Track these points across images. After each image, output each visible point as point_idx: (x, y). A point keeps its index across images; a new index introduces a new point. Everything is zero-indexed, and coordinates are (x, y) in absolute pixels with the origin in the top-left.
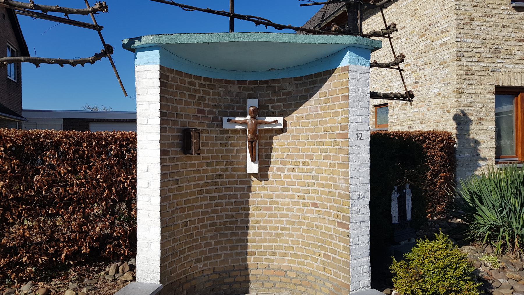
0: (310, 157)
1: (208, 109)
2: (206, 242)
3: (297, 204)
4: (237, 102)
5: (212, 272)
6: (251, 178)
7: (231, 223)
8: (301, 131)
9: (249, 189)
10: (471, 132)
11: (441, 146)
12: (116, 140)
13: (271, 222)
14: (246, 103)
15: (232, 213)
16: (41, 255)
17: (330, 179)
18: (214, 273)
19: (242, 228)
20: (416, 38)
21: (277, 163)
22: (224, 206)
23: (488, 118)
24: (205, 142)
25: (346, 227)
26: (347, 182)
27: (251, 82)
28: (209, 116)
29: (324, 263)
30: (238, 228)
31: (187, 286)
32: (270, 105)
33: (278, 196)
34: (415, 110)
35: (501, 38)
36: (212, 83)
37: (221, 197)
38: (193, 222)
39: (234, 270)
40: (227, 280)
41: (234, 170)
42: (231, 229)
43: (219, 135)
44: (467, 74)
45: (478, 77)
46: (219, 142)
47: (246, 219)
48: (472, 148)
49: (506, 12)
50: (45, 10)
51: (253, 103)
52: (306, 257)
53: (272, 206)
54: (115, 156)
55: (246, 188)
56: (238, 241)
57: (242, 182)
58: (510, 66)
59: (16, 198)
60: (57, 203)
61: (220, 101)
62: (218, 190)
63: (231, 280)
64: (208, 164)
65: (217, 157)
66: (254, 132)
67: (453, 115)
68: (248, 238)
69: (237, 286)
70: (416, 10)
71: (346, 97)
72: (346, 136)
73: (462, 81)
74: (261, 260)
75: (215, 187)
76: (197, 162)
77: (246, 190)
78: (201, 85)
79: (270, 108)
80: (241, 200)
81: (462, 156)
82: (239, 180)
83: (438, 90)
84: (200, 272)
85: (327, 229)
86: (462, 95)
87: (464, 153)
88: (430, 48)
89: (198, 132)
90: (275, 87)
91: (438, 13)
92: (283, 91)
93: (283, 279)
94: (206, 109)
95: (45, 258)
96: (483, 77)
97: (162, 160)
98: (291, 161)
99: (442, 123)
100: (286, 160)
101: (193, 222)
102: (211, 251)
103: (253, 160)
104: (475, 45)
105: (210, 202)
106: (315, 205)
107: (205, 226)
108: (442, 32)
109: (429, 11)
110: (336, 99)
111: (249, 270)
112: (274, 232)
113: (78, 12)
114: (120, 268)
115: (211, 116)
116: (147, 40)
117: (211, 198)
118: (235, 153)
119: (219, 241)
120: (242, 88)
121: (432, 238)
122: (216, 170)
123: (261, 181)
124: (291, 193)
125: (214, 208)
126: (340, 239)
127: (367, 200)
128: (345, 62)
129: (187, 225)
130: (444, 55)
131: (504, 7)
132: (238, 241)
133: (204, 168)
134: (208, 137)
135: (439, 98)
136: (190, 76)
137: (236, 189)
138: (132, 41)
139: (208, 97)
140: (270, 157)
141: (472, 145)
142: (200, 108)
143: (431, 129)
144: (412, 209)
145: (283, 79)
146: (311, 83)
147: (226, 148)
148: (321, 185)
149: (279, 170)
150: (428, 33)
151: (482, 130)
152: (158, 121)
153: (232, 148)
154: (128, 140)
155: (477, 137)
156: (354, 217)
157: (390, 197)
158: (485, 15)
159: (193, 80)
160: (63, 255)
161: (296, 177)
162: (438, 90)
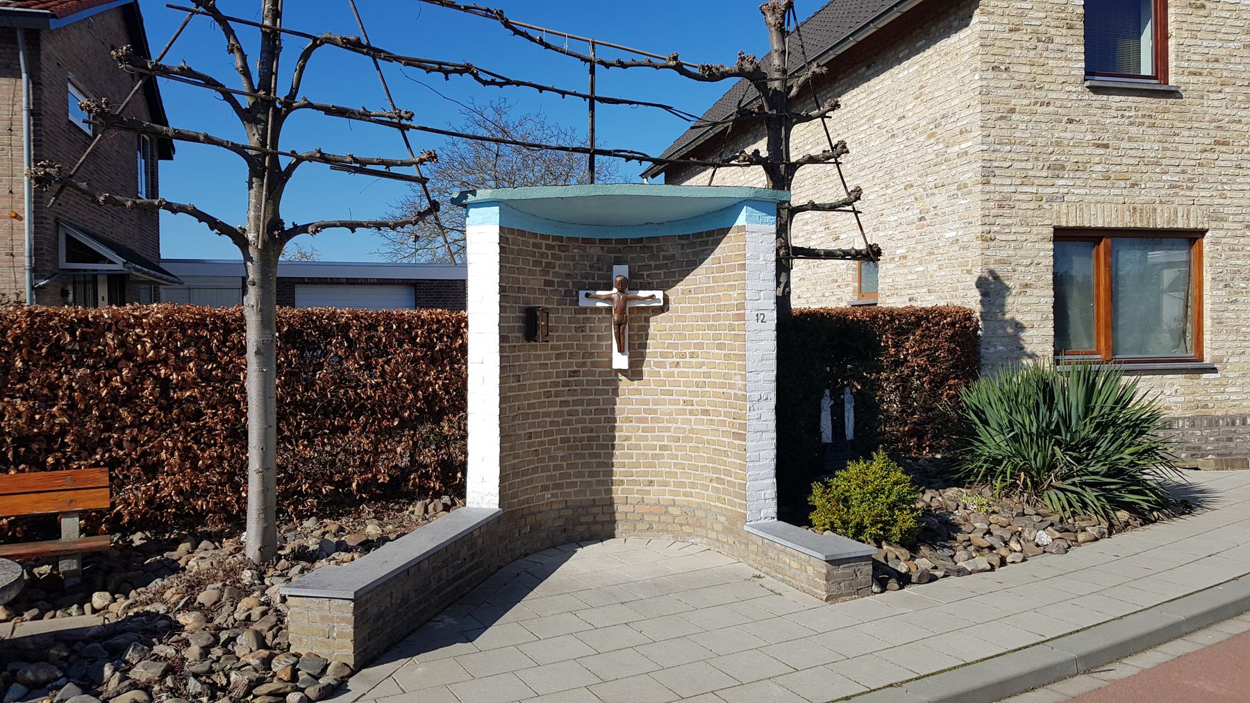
0: (700, 346)
3: (683, 412)
5: (563, 505)
7: (590, 439)
8: (688, 310)
9: (616, 392)
10: (1008, 308)
11: (950, 332)
12: (423, 321)
13: (646, 439)
14: (611, 270)
16: (324, 484)
17: (724, 376)
18: (567, 507)
19: (605, 447)
20: (922, 139)
23: (1041, 284)
25: (742, 437)
26: (744, 378)
27: (618, 241)
29: (716, 490)
30: (600, 447)
31: (530, 519)
33: (656, 402)
34: (921, 269)
35: (1066, 142)
37: (575, 403)
38: (538, 435)
40: (582, 519)
41: (594, 365)
44: (1000, 207)
45: (1021, 212)
48: (1009, 336)
49: (1074, 96)
50: (364, 163)
51: (620, 271)
52: (693, 485)
54: (422, 345)
56: (599, 465)
57: (605, 383)
58: (1083, 191)
59: (294, 402)
60: (345, 411)
62: (573, 393)
63: (590, 519)
64: (558, 356)
65: (571, 346)
67: (976, 279)
69: (598, 527)
70: (922, 87)
71: (743, 267)
72: (742, 317)
73: (991, 220)
74: (632, 492)
78: (549, 247)
81: (992, 350)
83: (954, 234)
85: (722, 444)
86: (992, 244)
87: (995, 346)
88: (942, 159)
89: (547, 312)
91: (955, 98)
93: (663, 518)
94: (556, 280)
95: (329, 487)
96: (1030, 212)
97: (502, 349)
99: (961, 293)
101: (538, 435)
102: (562, 476)
103: (621, 350)
104: (1016, 157)
106: (706, 412)
107: (553, 442)
108: (961, 133)
109: (942, 92)
110: (731, 268)
112: (650, 452)
113: (403, 164)
114: (431, 507)
116: (483, 194)
117: (563, 403)
121: (868, 457)
126: (737, 456)
127: (772, 403)
128: (741, 220)
129: (530, 438)
130: (964, 173)
131: (1071, 88)
132: (599, 465)
134: (559, 317)
135: (956, 248)
136: (535, 235)
137: (597, 392)
138: (463, 195)
139: (558, 263)
140: (645, 346)
141: (1010, 330)
143: (942, 304)
144: (856, 424)
146: (702, 243)
148: (714, 385)
149: (657, 364)
150: (939, 130)
151: (1027, 305)
152: (497, 298)
154: (439, 322)
155: (1019, 318)
156: (753, 425)
157: (819, 404)
158: (1036, 103)
159: (538, 241)
160: (354, 485)
161: (681, 374)
162: (954, 234)
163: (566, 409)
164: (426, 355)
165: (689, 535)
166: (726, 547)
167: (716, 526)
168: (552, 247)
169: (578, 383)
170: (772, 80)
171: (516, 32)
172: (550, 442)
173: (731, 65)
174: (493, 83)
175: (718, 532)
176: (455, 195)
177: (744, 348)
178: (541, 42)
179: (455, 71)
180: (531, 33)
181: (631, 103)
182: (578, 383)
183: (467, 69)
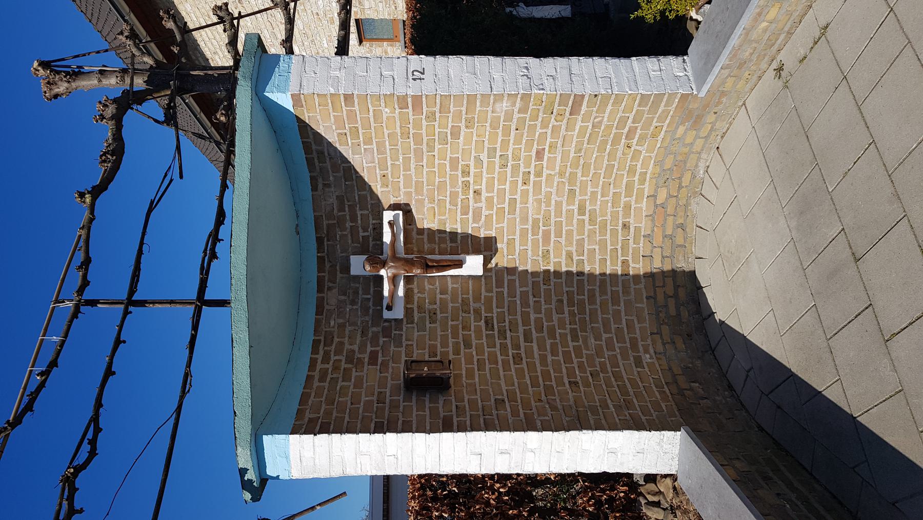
0: (454, 163)
1: (369, 345)
3: (537, 185)
4: (356, 292)
5: (657, 337)
7: (571, 303)
8: (408, 178)
9: (511, 271)
12: (423, 507)
13: (569, 233)
14: (357, 278)
15: (553, 303)
18: (659, 333)
19: (580, 284)
21: (464, 222)
22: (542, 316)
24: (427, 350)
26: (499, 98)
27: (320, 269)
28: (381, 342)
29: (642, 138)
30: (580, 290)
31: (682, 380)
33: (525, 220)
36: (322, 338)
37: (526, 322)
38: (571, 372)
41: (477, 299)
42: (581, 303)
46: (428, 325)
51: (358, 265)
52: (632, 171)
53: (541, 231)
55: (510, 277)
56: (603, 292)
57: (500, 284)
62: (513, 326)
63: (672, 303)
64: (468, 345)
66: (409, 263)
68: (598, 273)
71: (348, 98)
72: (417, 99)
75: (508, 332)
76: (463, 365)
77: (513, 278)
78: (326, 359)
79: (366, 234)
80: (530, 286)
82: (495, 290)
84: (658, 359)
90: (328, 226)
92: (335, 211)
93: (670, 210)
97: (462, 428)
98: (461, 197)
100: (459, 206)
101: (571, 372)
102: (621, 339)
103: (459, 264)
106: (540, 154)
107: (578, 350)
110: (351, 115)
111: (655, 271)
112: (587, 227)
114: (651, 498)
115: (382, 340)
116: (244, 459)
117: (528, 337)
118: (448, 297)
120: (331, 285)
123: (496, 250)
124: (518, 197)
125: (545, 334)
126: (601, 110)
128: (284, 100)
129: (576, 383)
132: (603, 292)
133: (474, 353)
134: (419, 346)
136: (309, 378)
137: (512, 294)
138: (247, 485)
140: (453, 235)
145: (314, 211)
147: (438, 312)
152: (391, 437)
153: (438, 302)
156: (562, 86)
157: (525, 19)
159: (316, 374)
161: (490, 188)
163: (535, 335)
164: (464, 504)
165: (694, 177)
166: (718, 125)
167: (688, 140)
170: (132, 84)
171: (29, 407)
172: (579, 355)
173: (108, 128)
174: (93, 442)
175: (697, 137)
176: (247, 496)
177: (459, 98)
178: (46, 373)
179: (71, 499)
180: (32, 388)
181: (140, 252)
183: (69, 483)
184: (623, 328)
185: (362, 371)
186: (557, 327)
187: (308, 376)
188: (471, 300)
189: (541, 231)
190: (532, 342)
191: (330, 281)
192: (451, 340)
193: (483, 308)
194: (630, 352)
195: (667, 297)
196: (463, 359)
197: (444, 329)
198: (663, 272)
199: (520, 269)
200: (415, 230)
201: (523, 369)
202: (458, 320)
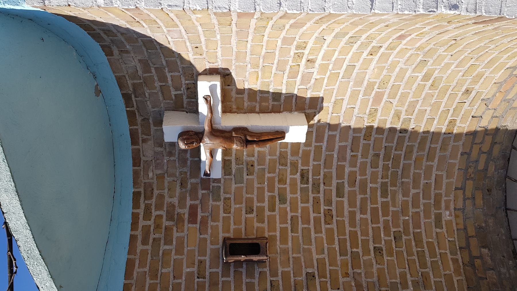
1: (188, 198)
2: (410, 205)
5: (460, 192)
6: (313, 125)
7: (387, 157)
9: (332, 127)
15: (370, 157)
18: (463, 188)
22: (357, 169)
24: (244, 205)
28: (200, 196)
31: (474, 242)
32: (173, 93)
36: (142, 190)
37: (340, 175)
39: (469, 154)
40: (481, 166)
42: (397, 159)
43: (232, 177)
46: (245, 177)
47: (386, 134)
61: (173, 175)
62: (327, 179)
64: (283, 200)
68: (421, 131)
75: (322, 185)
76: (278, 225)
77: (334, 133)
78: (147, 215)
80: (350, 141)
84: (456, 216)
90: (134, 85)
92: (140, 73)
94: (189, 202)
102: (426, 195)
105: (346, 195)
111: (479, 129)
115: (201, 192)
117: (340, 194)
119: (414, 181)
120: (145, 137)
122: (293, 184)
123: (321, 108)
125: (357, 188)
132: (421, 148)
133: (288, 209)
136: (133, 239)
137: (330, 148)
139: (167, 200)
142: (187, 216)
145: (114, 72)
147: (256, 164)
168: (148, 208)
169: (317, 172)
182: (317, 172)
184: (431, 183)
185: (183, 232)
186: (369, 181)
187: (128, 260)
188: (289, 154)
189: (374, 92)
190: (343, 197)
191: (143, 133)
192: (267, 194)
193: (300, 161)
194: (433, 209)
195: (481, 152)
196: (278, 217)
197: (261, 182)
198: (486, 130)
199: (343, 125)
200: (234, 90)
201: (332, 230)
202: (274, 172)
